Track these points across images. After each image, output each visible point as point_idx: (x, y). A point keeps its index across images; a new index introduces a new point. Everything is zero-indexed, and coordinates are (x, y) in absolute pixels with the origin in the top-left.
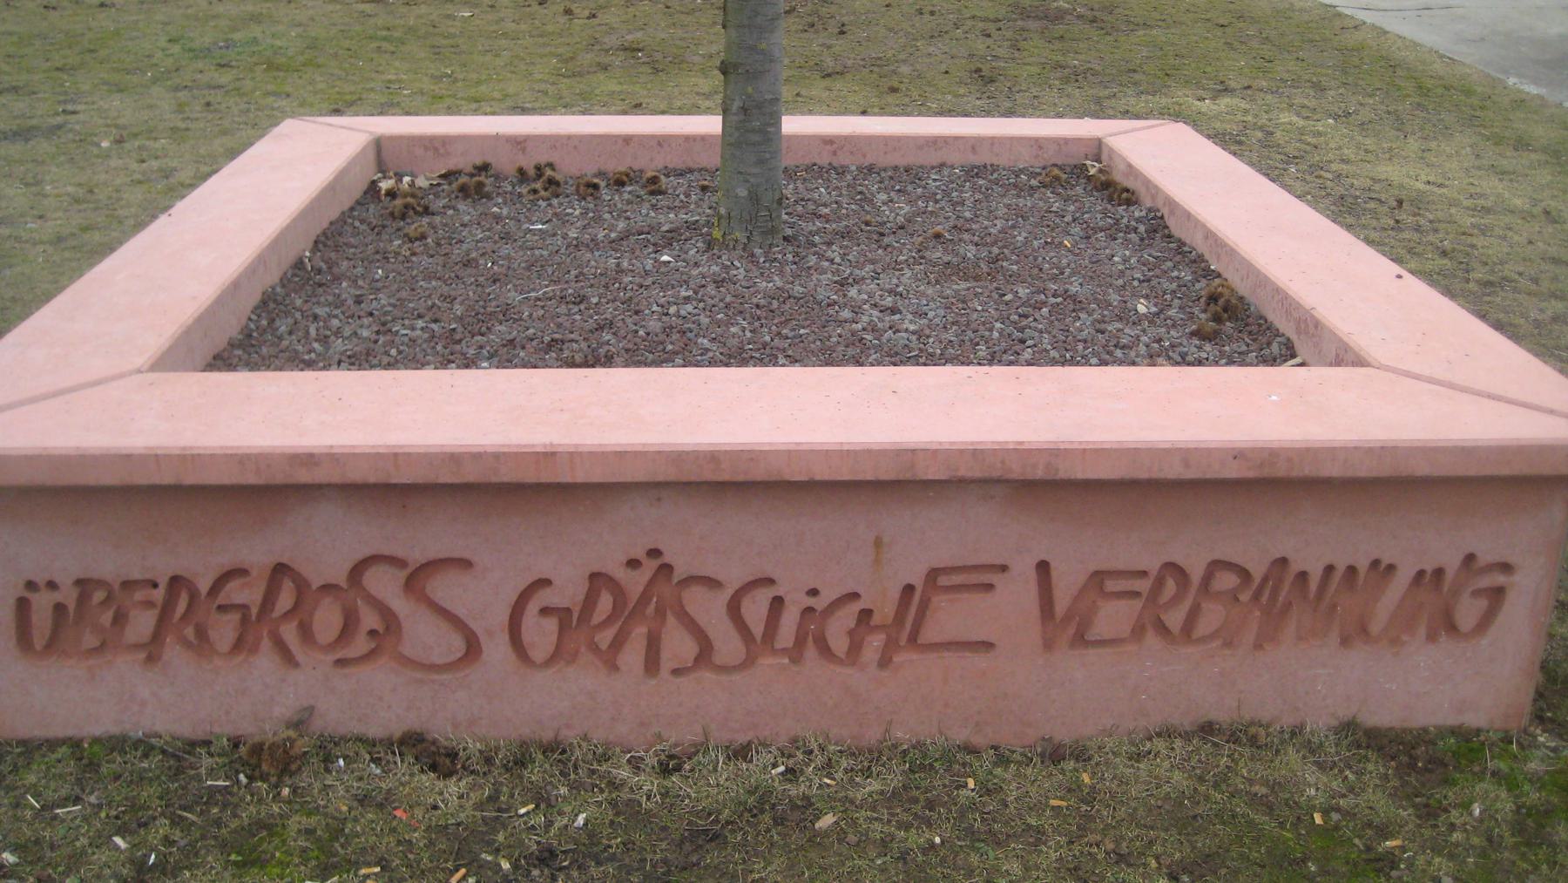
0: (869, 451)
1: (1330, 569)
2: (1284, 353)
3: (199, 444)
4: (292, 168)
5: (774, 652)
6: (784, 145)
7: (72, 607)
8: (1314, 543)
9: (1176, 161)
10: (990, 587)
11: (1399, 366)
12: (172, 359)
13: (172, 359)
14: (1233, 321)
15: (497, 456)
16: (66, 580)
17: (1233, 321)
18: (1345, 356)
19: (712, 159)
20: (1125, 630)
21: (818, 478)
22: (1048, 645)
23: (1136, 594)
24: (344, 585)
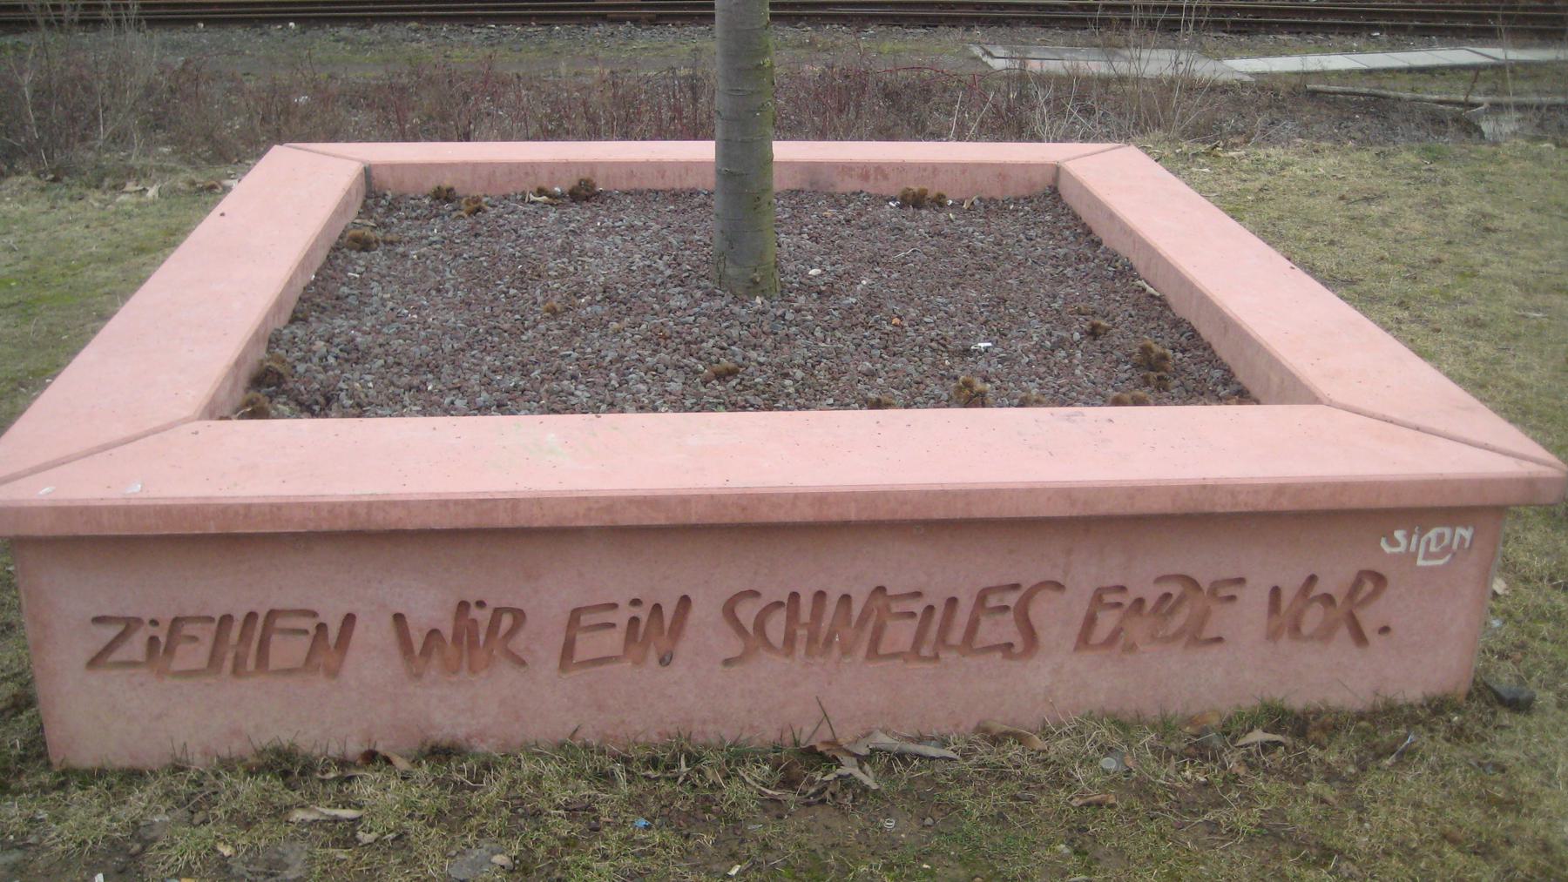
0: (945, 493)
1: (820, 596)
2: (1243, 396)
3: (521, 488)
4: (290, 199)
5: (951, 647)
6: (775, 169)
7: (163, 639)
8: (848, 574)
9: (1135, 190)
10: (1232, 598)
11: (1352, 400)
12: (214, 411)
13: (214, 411)
14: (1180, 357)
15: (370, 505)
16: (166, 617)
17: (1180, 357)
18: (1293, 391)
19: (710, 181)
20: (620, 652)
21: (1219, 509)
22: (1273, 635)
23: (912, 615)
24: (1205, 587)
